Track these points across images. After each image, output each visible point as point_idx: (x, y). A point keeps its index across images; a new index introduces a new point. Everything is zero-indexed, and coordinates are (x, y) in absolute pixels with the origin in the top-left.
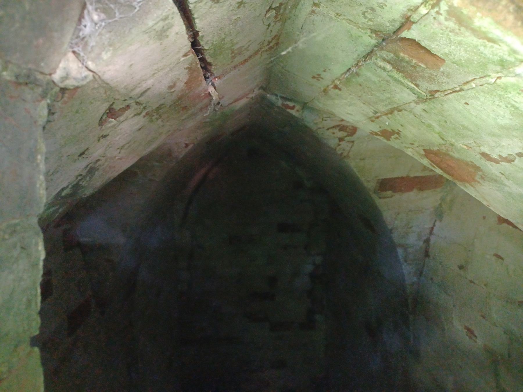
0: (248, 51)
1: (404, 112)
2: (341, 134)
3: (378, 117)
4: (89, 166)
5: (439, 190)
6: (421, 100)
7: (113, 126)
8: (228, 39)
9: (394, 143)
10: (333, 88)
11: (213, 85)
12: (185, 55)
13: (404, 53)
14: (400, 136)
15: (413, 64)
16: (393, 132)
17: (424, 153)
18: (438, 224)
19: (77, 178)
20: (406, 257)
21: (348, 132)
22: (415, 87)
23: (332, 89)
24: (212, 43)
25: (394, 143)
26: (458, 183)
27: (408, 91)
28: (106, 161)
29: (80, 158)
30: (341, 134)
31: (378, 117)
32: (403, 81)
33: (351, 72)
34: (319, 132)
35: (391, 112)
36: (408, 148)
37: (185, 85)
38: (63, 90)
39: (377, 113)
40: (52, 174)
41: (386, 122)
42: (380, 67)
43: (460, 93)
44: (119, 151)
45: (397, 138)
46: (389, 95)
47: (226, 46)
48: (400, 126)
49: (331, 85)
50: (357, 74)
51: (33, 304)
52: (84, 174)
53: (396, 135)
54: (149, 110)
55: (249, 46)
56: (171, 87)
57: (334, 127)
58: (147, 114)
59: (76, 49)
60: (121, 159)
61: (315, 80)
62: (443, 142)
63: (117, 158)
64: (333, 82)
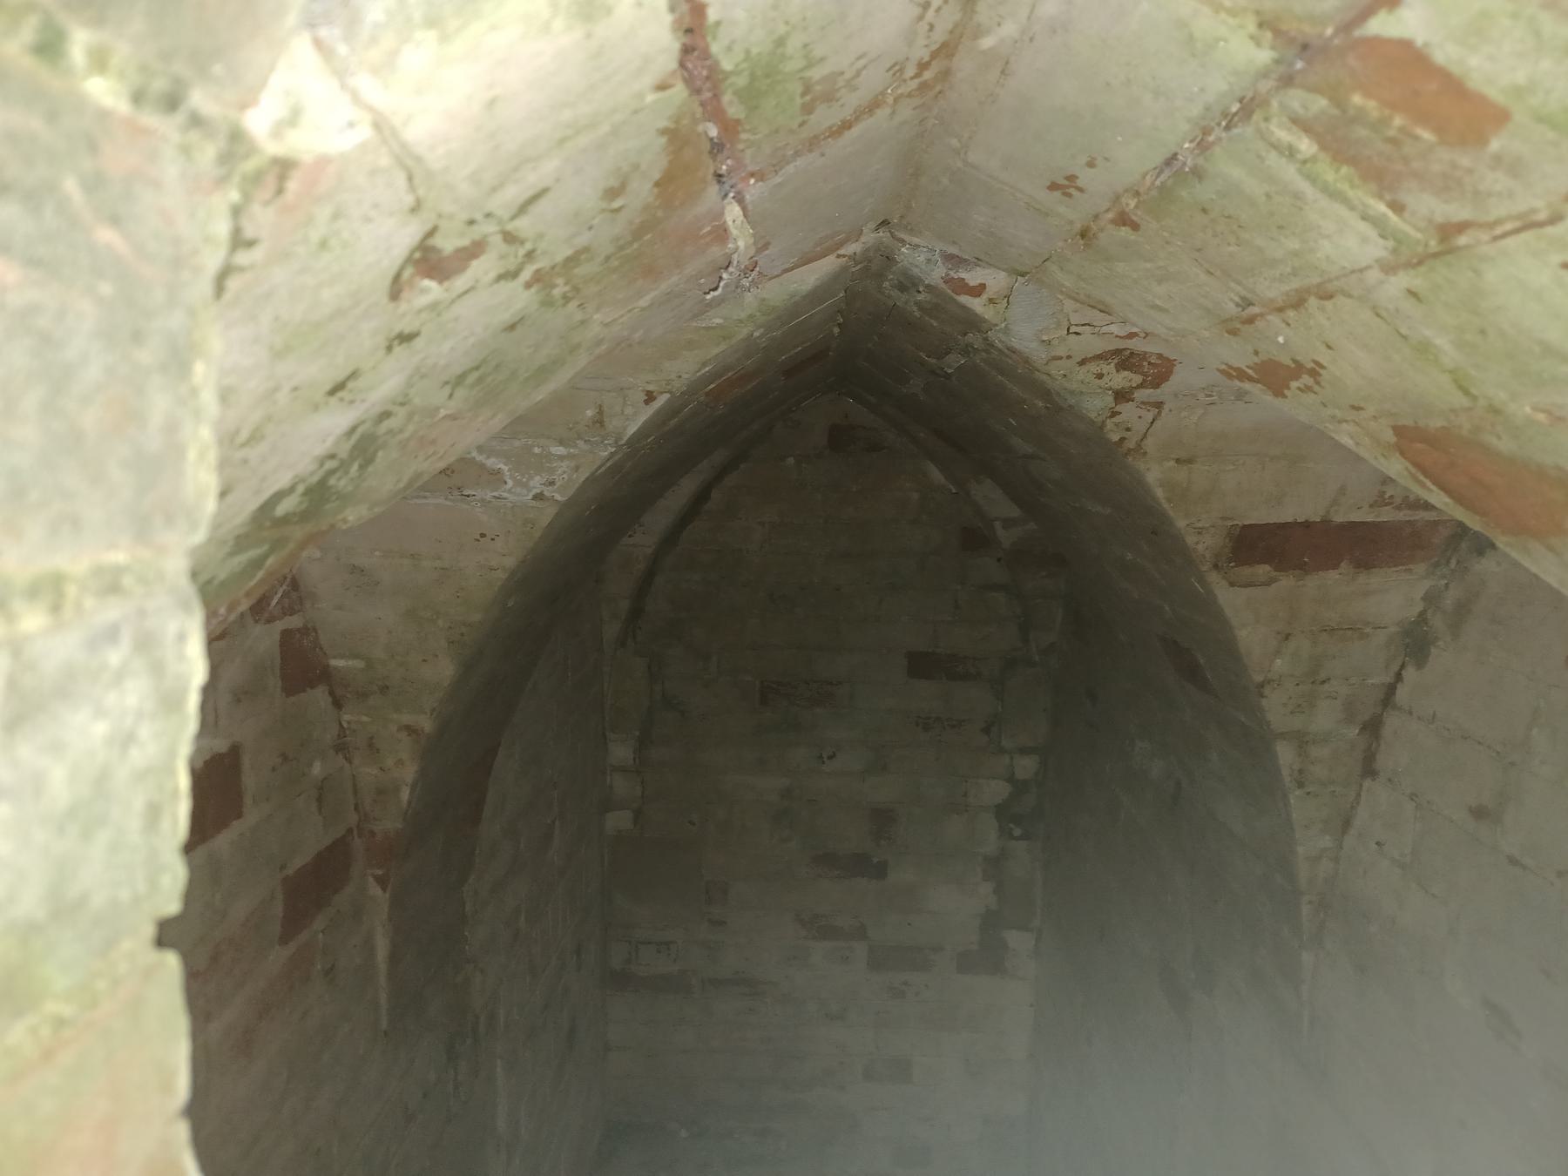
0: (854, 89)
1: (1340, 300)
2: (1121, 379)
3: (1251, 320)
4: (360, 431)
5: (1420, 568)
6: (1402, 260)
7: (434, 307)
8: (794, 44)
9: (1297, 406)
10: (1113, 221)
11: (740, 199)
12: (662, 87)
13: (1367, 94)
14: (1318, 383)
15: (1391, 133)
16: (1298, 369)
17: (1393, 439)
18: (1410, 673)
19: (322, 465)
20: (1301, 771)
21: (1145, 375)
22: (1390, 213)
23: (1110, 226)
24: (748, 52)
25: (1297, 406)
26: (1501, 541)
27: (1363, 227)
28: (410, 416)
29: (333, 400)
30: (1121, 379)
31: (1251, 320)
32: (1351, 193)
33: (1177, 165)
34: (1056, 369)
35: (1297, 302)
36: (1340, 422)
37: (656, 190)
38: (284, 167)
39: (1251, 304)
40: (243, 445)
41: (1277, 335)
42: (1276, 146)
43: (1549, 230)
44: (447, 390)
45: (1308, 389)
46: (1293, 244)
47: (790, 66)
48: (1323, 348)
49: (1107, 211)
50: (1198, 173)
51: (165, 824)
52: (343, 453)
53: (1306, 380)
54: (541, 263)
55: (858, 73)
56: (612, 193)
57: (1099, 357)
58: (538, 278)
59: (323, 32)
60: (452, 418)
61: (1057, 194)
62: (1465, 402)
63: (443, 412)
64: (1117, 198)
